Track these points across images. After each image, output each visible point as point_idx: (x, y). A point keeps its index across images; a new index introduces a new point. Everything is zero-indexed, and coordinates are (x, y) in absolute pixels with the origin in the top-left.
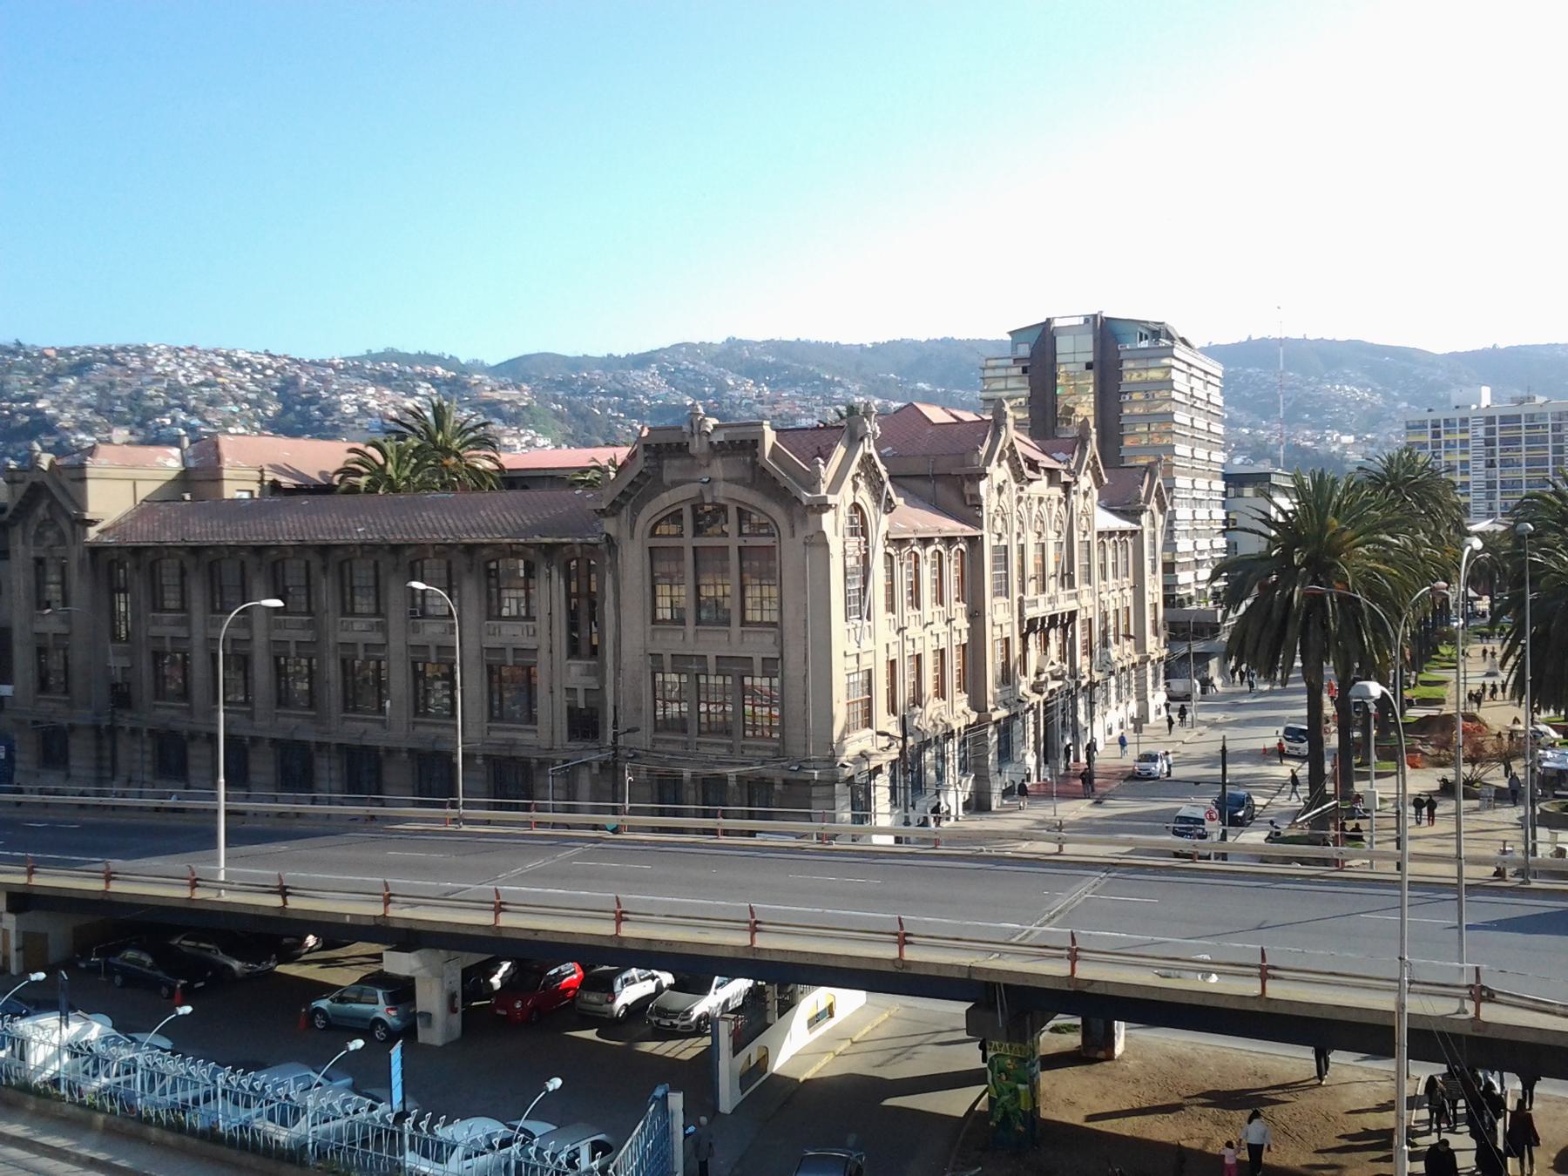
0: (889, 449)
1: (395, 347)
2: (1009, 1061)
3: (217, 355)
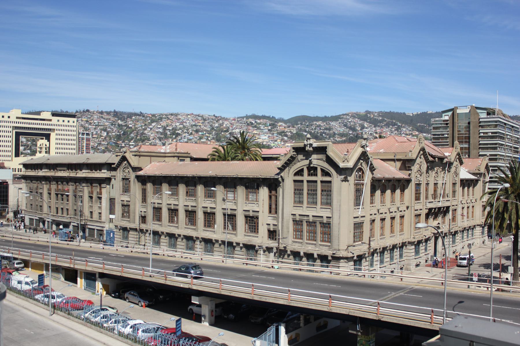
0: (383, 150)
1: (255, 113)
2: (364, 341)
3: (199, 116)
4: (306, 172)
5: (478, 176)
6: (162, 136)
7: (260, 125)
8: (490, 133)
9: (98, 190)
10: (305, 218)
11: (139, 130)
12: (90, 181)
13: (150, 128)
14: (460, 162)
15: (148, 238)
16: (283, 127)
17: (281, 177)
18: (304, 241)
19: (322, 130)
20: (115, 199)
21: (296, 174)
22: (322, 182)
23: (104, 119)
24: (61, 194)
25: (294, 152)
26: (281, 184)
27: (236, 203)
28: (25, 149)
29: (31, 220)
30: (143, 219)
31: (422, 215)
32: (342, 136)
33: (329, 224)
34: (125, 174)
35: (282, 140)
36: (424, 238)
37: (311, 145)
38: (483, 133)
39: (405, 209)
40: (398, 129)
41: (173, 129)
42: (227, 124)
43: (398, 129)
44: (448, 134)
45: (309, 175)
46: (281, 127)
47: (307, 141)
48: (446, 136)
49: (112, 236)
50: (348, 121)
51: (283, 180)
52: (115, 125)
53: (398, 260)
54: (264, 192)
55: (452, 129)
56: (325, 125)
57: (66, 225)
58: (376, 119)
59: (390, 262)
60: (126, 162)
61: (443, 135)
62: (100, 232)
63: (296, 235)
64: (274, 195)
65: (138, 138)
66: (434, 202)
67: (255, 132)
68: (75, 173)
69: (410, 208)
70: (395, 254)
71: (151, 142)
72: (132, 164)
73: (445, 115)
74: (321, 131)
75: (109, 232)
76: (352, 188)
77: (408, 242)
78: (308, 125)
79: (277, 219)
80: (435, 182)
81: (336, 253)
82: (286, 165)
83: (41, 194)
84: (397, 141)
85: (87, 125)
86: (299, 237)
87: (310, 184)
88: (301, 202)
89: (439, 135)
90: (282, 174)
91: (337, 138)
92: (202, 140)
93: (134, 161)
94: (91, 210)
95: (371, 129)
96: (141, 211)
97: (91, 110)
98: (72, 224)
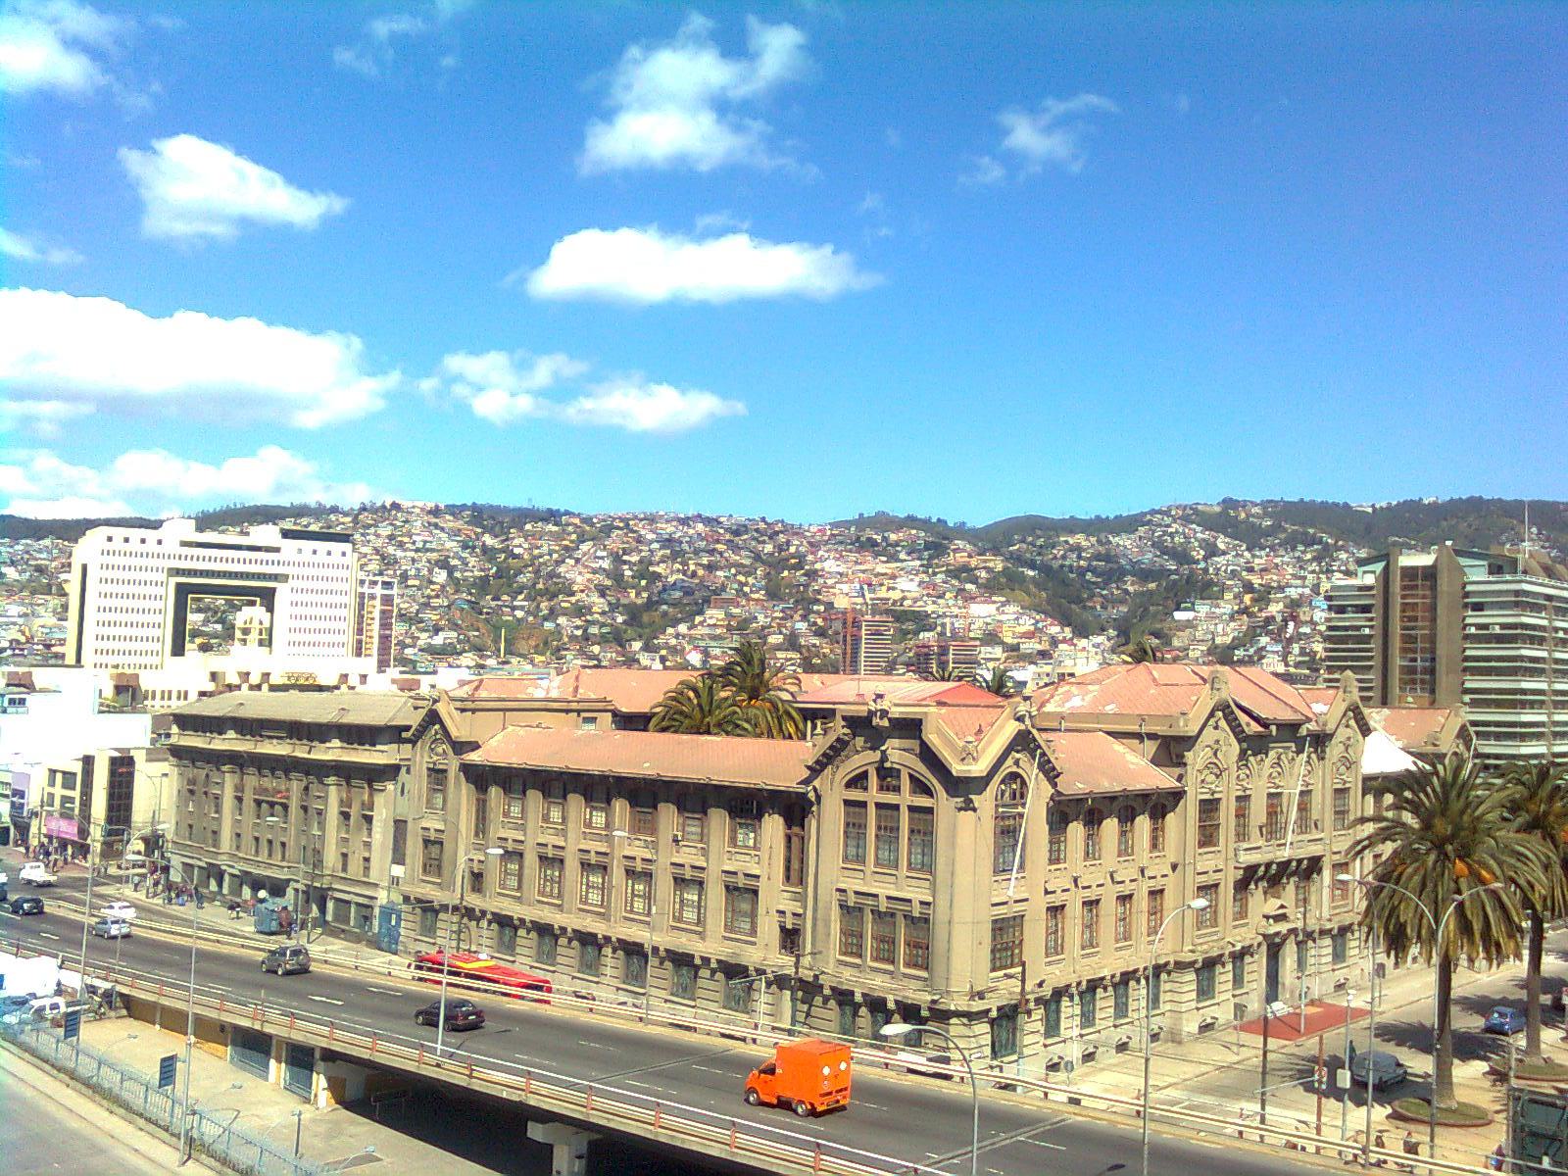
4: (873, 780)
6: (608, 583)
8: (1497, 627)
9: (366, 797)
11: (540, 564)
12: (347, 772)
14: (1360, 727)
15: (485, 933)
17: (815, 789)
19: (1085, 559)
20: (406, 822)
21: (850, 784)
22: (912, 809)
23: (442, 529)
24: (267, 802)
26: (814, 808)
27: (705, 852)
28: (206, 622)
29: (188, 867)
30: (477, 879)
31: (1222, 888)
32: (1147, 577)
33: (927, 921)
34: (435, 758)
37: (884, 713)
38: (1479, 626)
39: (1168, 870)
40: (1325, 555)
41: (641, 561)
42: (801, 545)
43: (1325, 555)
44: (1371, 627)
45: (881, 789)
46: (961, 553)
48: (1367, 631)
49: (393, 923)
50: (1165, 533)
51: (818, 797)
52: (474, 547)
53: (1077, 1031)
54: (773, 826)
56: (1093, 545)
57: (278, 889)
58: (1253, 525)
59: (1115, 1019)
60: (437, 727)
61: (1358, 628)
62: (364, 912)
63: (846, 944)
64: (797, 835)
65: (540, 586)
66: (1264, 849)
67: (881, 568)
68: (308, 748)
69: (1179, 868)
70: (1099, 1004)
71: (578, 601)
72: (454, 733)
73: (1365, 572)
74: (1082, 563)
75: (387, 912)
76: (988, 826)
77: (1176, 963)
78: (1041, 546)
79: (801, 898)
80: (1273, 791)
82: (825, 760)
83: (217, 797)
84: (1154, 680)
85: (391, 550)
87: (883, 812)
88: (860, 859)
89: (1346, 628)
90: (816, 783)
91: (1132, 585)
93: (459, 727)
94: (345, 850)
95: (1237, 555)
96: (472, 860)
97: (405, 504)
98: (293, 885)
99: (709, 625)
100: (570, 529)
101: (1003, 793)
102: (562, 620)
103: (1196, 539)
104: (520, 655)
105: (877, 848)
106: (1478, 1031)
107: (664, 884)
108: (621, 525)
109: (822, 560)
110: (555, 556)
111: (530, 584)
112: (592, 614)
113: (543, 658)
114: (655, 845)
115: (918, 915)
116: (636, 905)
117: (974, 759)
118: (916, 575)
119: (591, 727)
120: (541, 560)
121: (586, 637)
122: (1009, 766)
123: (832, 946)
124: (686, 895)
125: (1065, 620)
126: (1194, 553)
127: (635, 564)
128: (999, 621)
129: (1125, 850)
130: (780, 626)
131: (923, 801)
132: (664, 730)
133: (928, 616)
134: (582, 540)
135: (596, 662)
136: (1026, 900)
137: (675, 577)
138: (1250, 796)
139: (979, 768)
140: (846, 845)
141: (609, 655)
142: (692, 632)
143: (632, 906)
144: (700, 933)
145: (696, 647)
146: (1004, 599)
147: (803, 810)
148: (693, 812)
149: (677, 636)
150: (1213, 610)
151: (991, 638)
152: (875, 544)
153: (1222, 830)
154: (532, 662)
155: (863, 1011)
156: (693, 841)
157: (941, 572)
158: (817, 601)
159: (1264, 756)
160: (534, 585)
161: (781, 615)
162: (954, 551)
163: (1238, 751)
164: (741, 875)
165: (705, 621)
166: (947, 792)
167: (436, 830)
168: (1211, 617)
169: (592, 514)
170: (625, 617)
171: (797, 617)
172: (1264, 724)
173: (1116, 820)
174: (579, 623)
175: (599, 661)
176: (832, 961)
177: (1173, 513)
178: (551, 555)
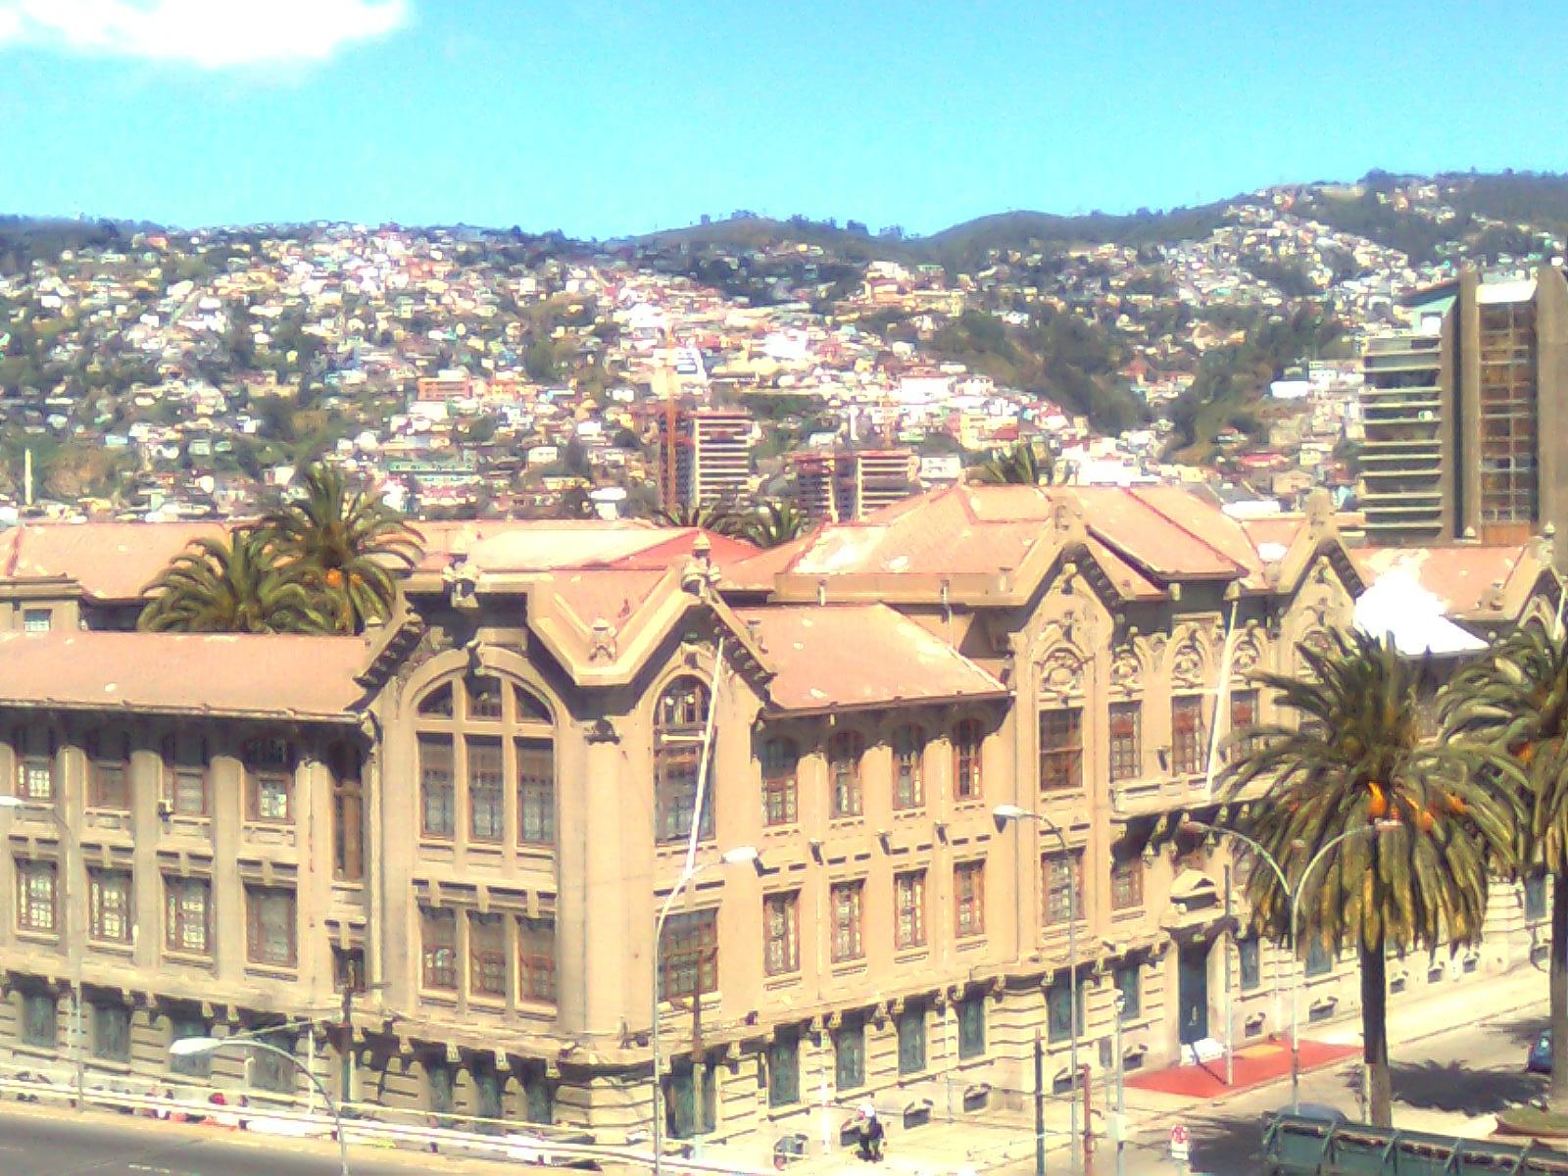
4: (461, 698)
5: (1492, 635)
7: (772, 280)
10: (461, 896)
11: (93, 326)
13: (158, 313)
16: (894, 288)
17: (372, 716)
18: (461, 996)
25: (415, 611)
26: (374, 750)
27: (209, 831)
33: (551, 924)
35: (883, 358)
36: (1106, 953)
37: (468, 586)
39: (989, 828)
44: (1435, 409)
47: (452, 566)
48: (1428, 416)
50: (1262, 239)
51: (378, 729)
53: (954, 1062)
54: (313, 780)
55: (1450, 381)
58: (1421, 218)
61: (1414, 412)
64: (350, 795)
65: (95, 367)
71: (168, 393)
76: (642, 765)
79: (360, 898)
81: (578, 1050)
82: (384, 669)
86: (447, 980)
88: (447, 829)
90: (374, 706)
92: (444, 375)
99: (417, 433)
100: (148, 257)
101: (670, 711)
102: (139, 431)
103: (1317, 249)
104: (65, 499)
105: (473, 811)
106: (1519, 1070)
107: (149, 889)
108: (246, 248)
109: (627, 305)
110: (121, 310)
111: (75, 363)
112: (195, 418)
113: (105, 504)
114: (130, 823)
115: (536, 916)
116: (107, 925)
117: (610, 656)
118: (803, 328)
119: (39, 628)
120: (94, 318)
121: (187, 462)
122: (676, 666)
123: (410, 974)
124: (185, 905)
125: (1075, 400)
126: (1314, 274)
127: (273, 322)
128: (952, 410)
129: (905, 803)
130: (549, 430)
131: (537, 730)
132: (167, 627)
133: (823, 404)
134: (171, 277)
135: (207, 508)
136: (720, 884)
137: (350, 344)
138: (1139, 702)
139: (618, 671)
140: (426, 808)
141: (232, 494)
142: (387, 446)
143: (102, 928)
144: (208, 967)
145: (394, 475)
146: (962, 368)
147: (358, 752)
148: (188, 764)
149: (358, 454)
150: (1343, 377)
151: (940, 441)
152: (730, 273)
153: (1086, 761)
154: (85, 510)
155: (463, 1075)
156: (191, 814)
157: (848, 322)
158: (620, 382)
159: (1163, 636)
160: (83, 366)
161: (553, 409)
162: (874, 282)
163: (1111, 629)
164: (267, 868)
165: (409, 425)
166: (572, 712)
167: (41, 841)
168: (1338, 391)
169: (188, 228)
170: (258, 422)
171: (581, 412)
172: (1159, 581)
173: (888, 751)
174: (170, 434)
175: (214, 506)
176: (412, 998)
177: (1277, 200)
178: (112, 308)
